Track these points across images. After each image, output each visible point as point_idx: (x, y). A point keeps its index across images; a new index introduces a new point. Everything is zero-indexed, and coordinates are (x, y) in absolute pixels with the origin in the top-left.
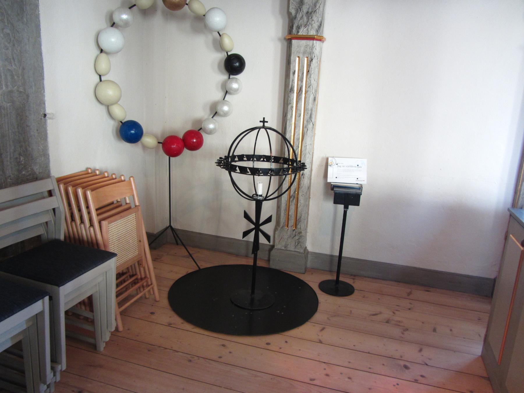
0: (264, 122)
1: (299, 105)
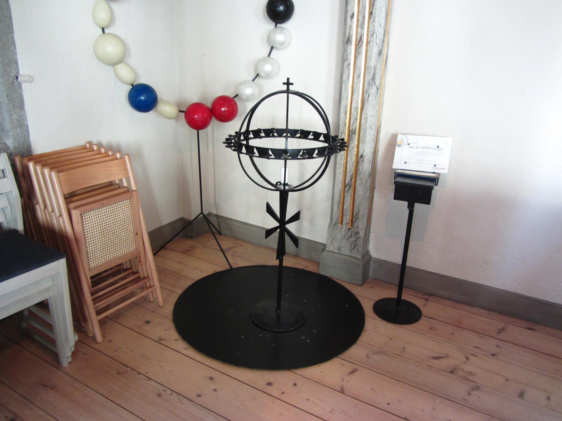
0: (288, 84)
1: (358, 61)
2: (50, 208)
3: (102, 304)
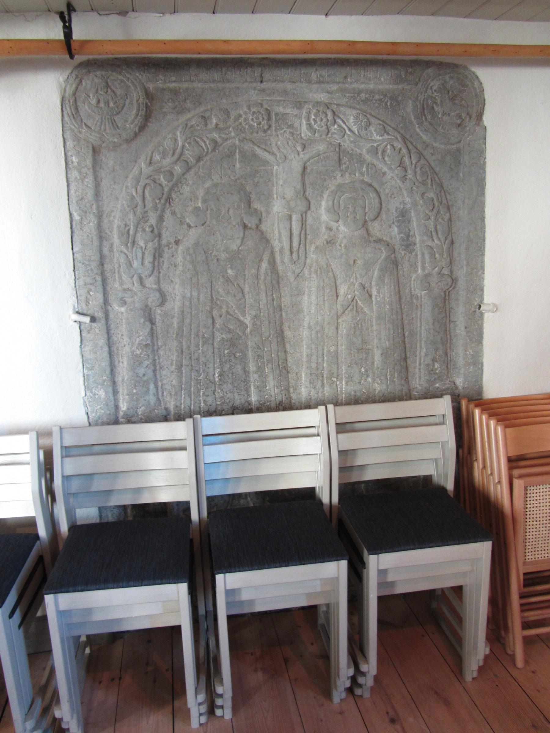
2: (489, 469)
3: (533, 615)
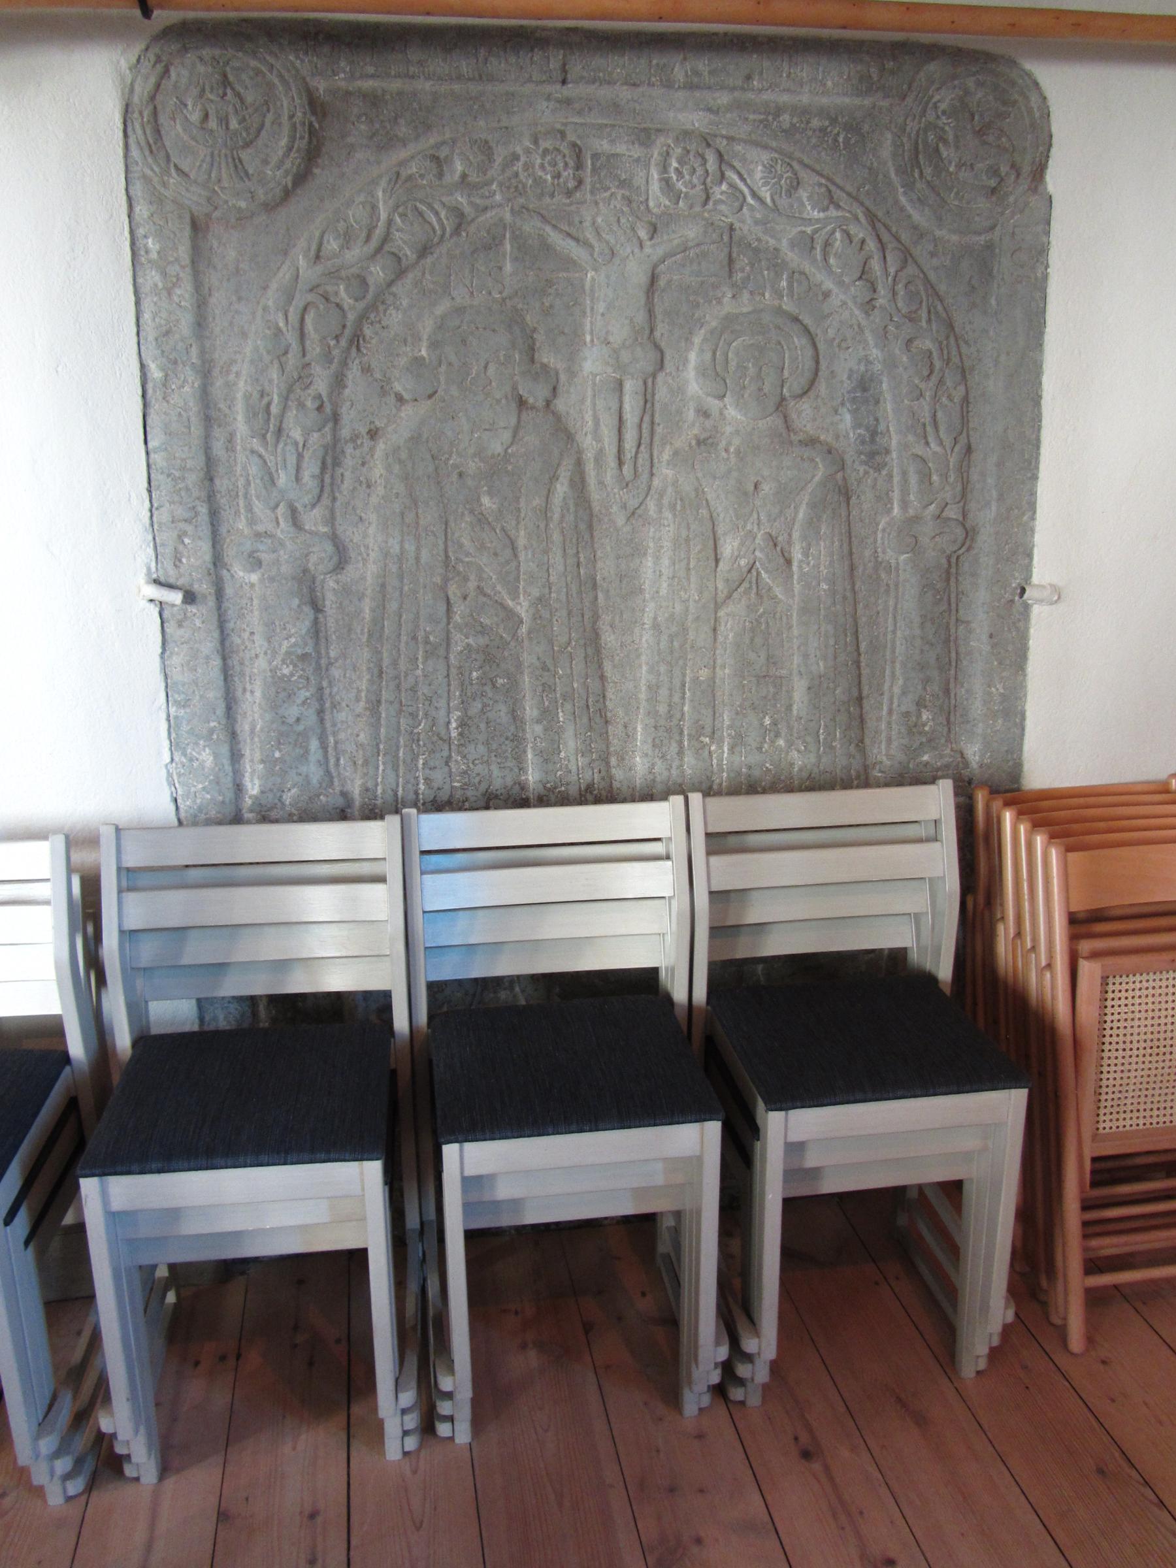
3: (1109, 1246)
